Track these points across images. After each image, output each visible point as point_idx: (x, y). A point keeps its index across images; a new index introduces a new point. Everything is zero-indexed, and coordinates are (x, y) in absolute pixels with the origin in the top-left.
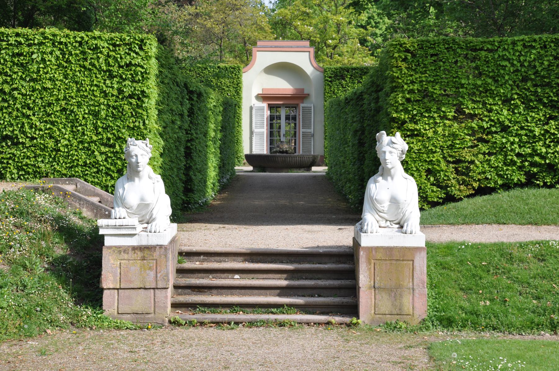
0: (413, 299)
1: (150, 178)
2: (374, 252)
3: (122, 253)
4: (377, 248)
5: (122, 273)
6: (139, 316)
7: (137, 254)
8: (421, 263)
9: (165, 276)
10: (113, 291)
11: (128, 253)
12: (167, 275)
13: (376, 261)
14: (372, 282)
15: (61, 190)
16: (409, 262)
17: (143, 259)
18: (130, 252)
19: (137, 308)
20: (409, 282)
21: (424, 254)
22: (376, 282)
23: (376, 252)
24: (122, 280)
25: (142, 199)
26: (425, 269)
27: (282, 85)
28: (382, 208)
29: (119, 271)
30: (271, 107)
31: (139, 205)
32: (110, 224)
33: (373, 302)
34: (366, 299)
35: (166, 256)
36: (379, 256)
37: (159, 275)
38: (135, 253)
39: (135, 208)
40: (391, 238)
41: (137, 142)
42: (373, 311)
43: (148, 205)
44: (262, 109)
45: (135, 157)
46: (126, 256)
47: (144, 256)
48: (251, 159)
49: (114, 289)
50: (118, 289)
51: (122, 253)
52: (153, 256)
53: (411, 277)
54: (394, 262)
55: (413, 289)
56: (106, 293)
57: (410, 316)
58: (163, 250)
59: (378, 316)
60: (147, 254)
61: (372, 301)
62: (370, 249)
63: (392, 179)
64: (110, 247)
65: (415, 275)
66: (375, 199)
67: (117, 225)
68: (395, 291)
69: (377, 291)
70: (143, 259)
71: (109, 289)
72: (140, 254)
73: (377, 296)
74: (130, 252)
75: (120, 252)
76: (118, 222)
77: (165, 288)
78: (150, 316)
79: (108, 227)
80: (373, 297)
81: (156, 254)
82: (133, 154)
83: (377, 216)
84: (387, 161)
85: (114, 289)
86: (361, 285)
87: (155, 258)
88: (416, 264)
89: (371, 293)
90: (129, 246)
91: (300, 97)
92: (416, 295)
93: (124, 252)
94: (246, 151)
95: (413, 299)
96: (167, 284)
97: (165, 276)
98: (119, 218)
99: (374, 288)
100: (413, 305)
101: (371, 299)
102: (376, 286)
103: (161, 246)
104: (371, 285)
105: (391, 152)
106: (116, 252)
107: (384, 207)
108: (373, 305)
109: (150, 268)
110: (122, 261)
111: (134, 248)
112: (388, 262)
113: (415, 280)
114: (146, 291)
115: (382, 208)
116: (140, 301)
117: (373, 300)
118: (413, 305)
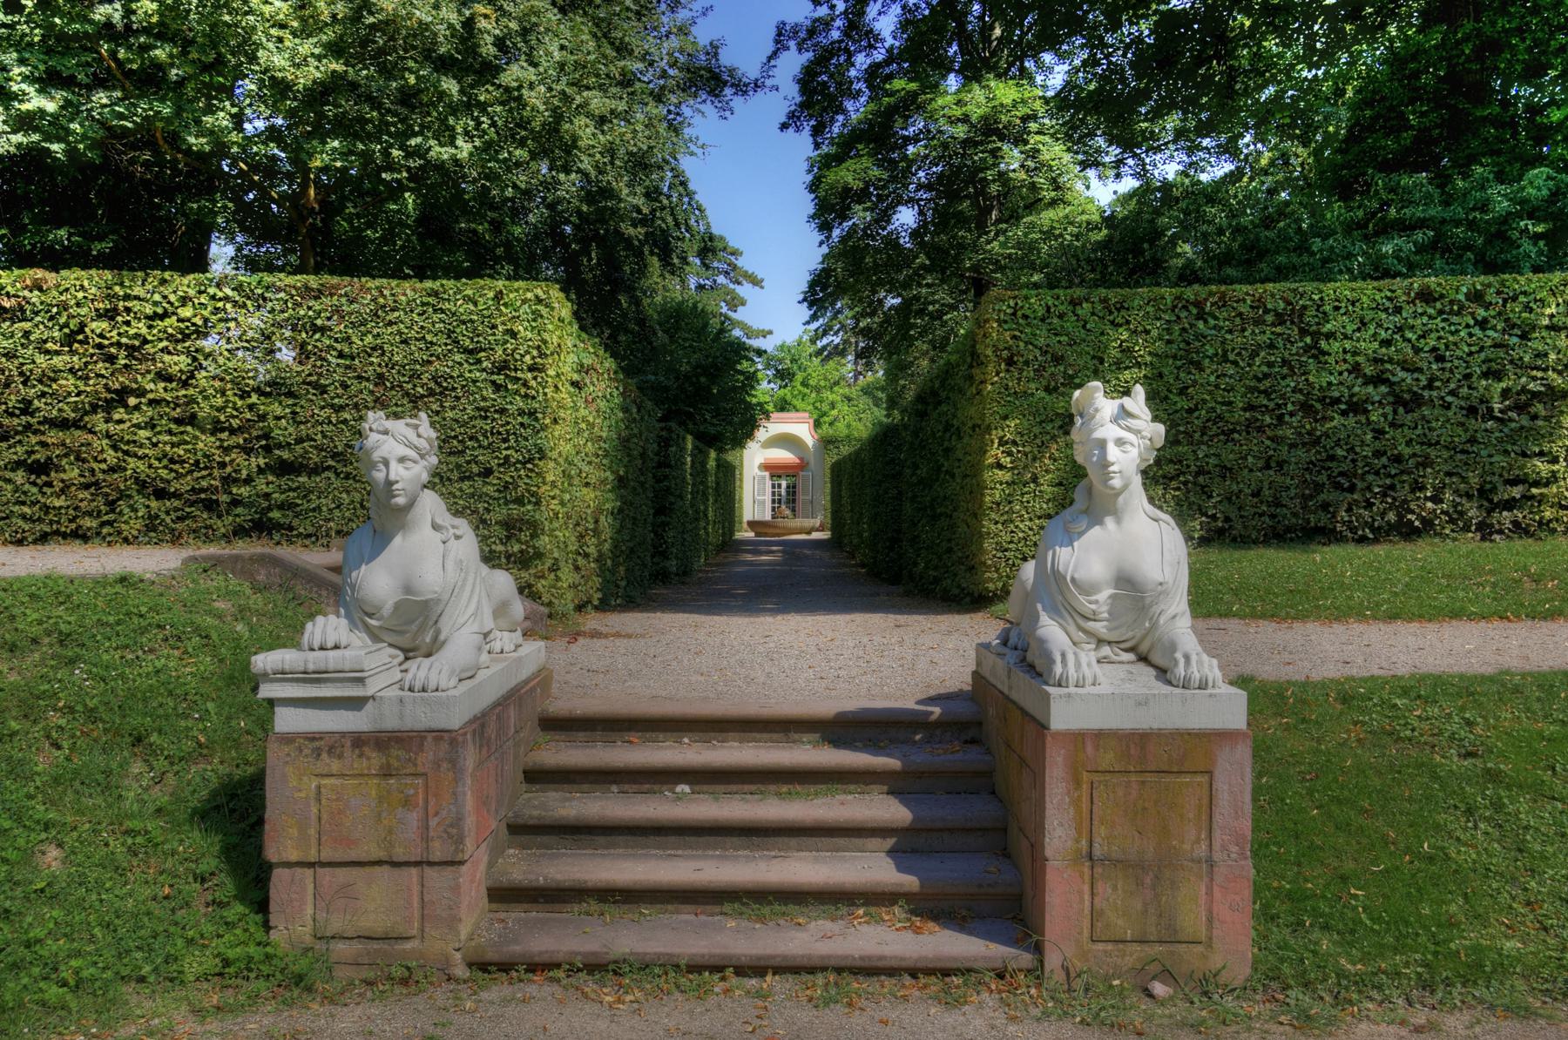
0: (1210, 893)
1: (436, 527)
2: (1089, 749)
3: (324, 756)
4: (1099, 736)
5: (325, 816)
6: (376, 945)
7: (368, 759)
8: (1234, 779)
9: (451, 826)
10: (299, 870)
11: (340, 757)
12: (458, 821)
13: (1096, 777)
14: (1084, 842)
15: (275, 561)
16: (1199, 778)
17: (386, 773)
18: (348, 752)
19: (373, 919)
20: (1198, 841)
21: (1243, 753)
22: (1097, 840)
23: (1097, 748)
24: (324, 839)
25: (408, 589)
26: (1248, 798)
27: (783, 455)
28: (1093, 607)
29: (315, 810)
30: (772, 476)
31: (398, 606)
32: (287, 668)
33: (1087, 903)
34: (1065, 898)
35: (453, 762)
36: (1107, 759)
37: (433, 822)
38: (360, 756)
39: (387, 610)
40: (1143, 702)
41: (390, 424)
42: (1086, 933)
43: (426, 606)
44: (763, 478)
45: (382, 467)
46: (335, 766)
47: (389, 765)
48: (753, 525)
49: (300, 864)
50: (311, 865)
51: (324, 756)
52: (415, 765)
53: (1204, 825)
54: (1149, 778)
55: (1211, 863)
56: (279, 877)
57: (1200, 948)
58: (445, 746)
59: (1101, 946)
60: (398, 758)
61: (1082, 901)
62: (1078, 739)
63: (1118, 521)
64: (288, 739)
65: (1217, 818)
66: (1073, 580)
67: (311, 667)
68: (1151, 872)
69: (1098, 870)
70: (386, 773)
71: (288, 865)
72: (375, 760)
73: (1100, 887)
74: (348, 752)
75: (317, 753)
76: (314, 660)
77: (452, 863)
78: (408, 946)
79: (283, 676)
80: (1086, 888)
81: (426, 759)
82: (376, 456)
83: (1072, 628)
84: (1111, 469)
85: (300, 864)
86: (1048, 852)
87: (420, 769)
88: (1221, 785)
89: (1082, 877)
90: (343, 734)
91: (803, 465)
92: (1218, 879)
93: (330, 752)
94: (745, 519)
95: (1210, 893)
96: (457, 851)
97: (451, 826)
98: (322, 648)
99: (1090, 857)
100: (1210, 911)
101: (1081, 893)
102: (1097, 852)
103: (440, 734)
104: (1079, 851)
105: (1120, 442)
106: (306, 751)
107: (1096, 602)
108: (1087, 911)
109: (407, 803)
110: (326, 781)
111: (359, 741)
112: (1133, 778)
113: (1217, 834)
114: (396, 872)
115: (1093, 607)
116: (378, 902)
117: (1087, 897)
118: (1210, 911)
